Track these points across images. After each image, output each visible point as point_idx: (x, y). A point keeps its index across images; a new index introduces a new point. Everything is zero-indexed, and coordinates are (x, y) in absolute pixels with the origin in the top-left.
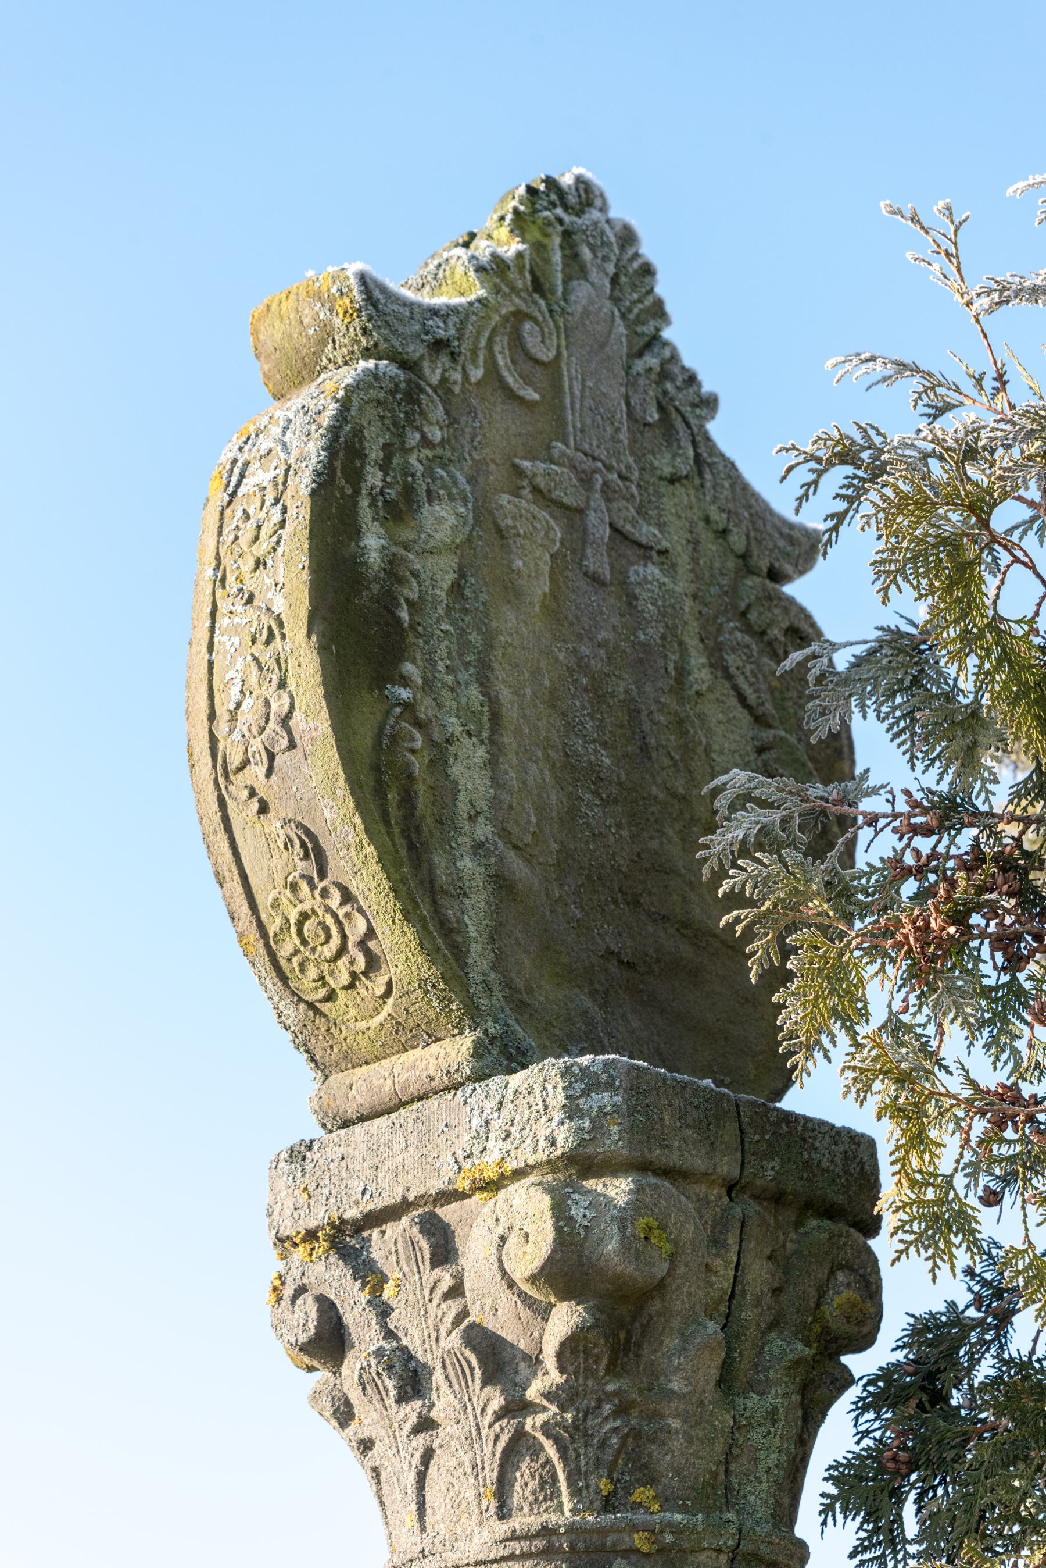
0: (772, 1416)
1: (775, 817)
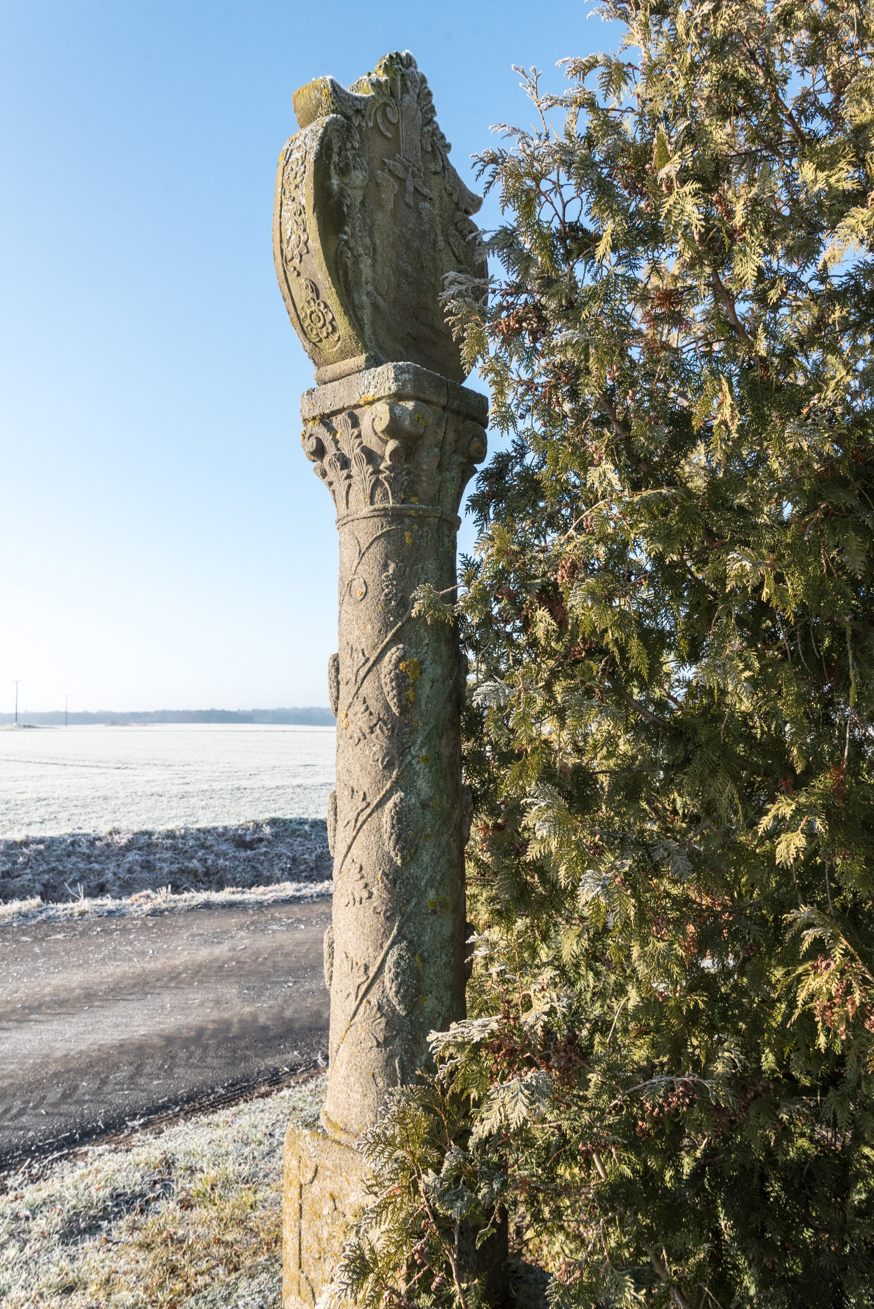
0: (453, 479)
1: (464, 287)
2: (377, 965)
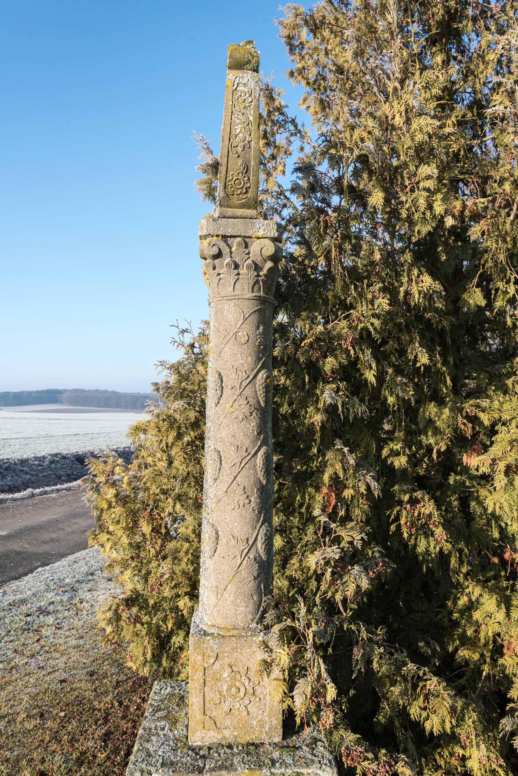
2: (254, 537)
